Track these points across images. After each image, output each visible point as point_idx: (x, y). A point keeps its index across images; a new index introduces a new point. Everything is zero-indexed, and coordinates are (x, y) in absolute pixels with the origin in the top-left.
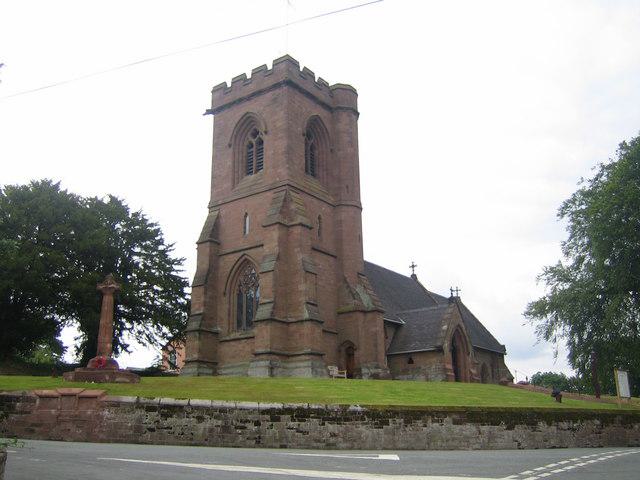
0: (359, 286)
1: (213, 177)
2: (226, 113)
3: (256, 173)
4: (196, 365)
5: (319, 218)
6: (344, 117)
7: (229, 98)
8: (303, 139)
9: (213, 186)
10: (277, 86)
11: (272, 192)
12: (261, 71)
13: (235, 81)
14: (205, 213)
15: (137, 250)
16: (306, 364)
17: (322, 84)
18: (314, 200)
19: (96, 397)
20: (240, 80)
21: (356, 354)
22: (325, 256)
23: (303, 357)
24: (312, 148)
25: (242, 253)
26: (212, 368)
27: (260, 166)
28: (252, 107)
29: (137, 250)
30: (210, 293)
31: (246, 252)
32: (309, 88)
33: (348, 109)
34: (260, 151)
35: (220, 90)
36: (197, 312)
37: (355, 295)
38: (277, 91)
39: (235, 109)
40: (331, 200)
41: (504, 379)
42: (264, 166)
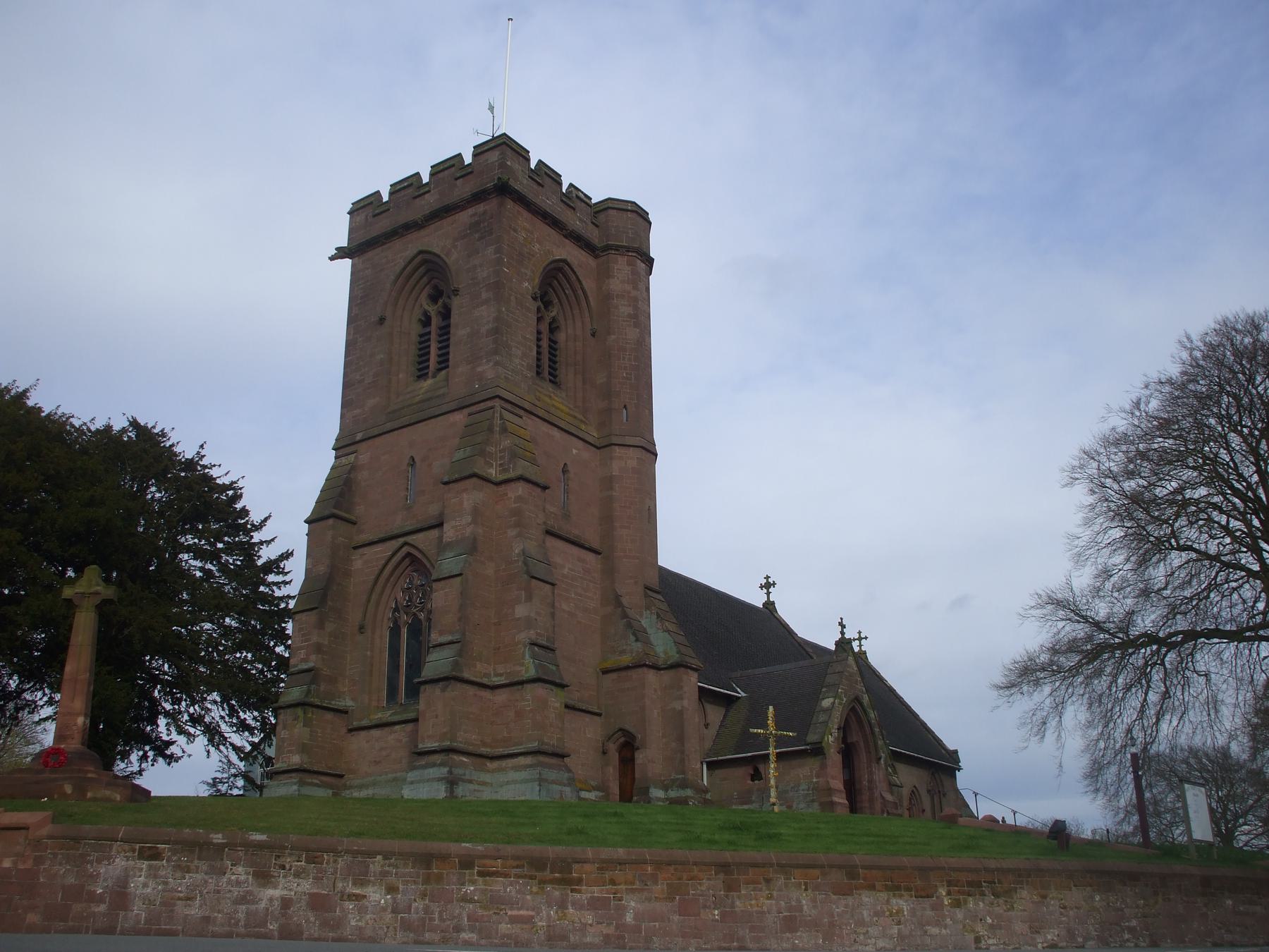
0: (646, 613)
1: (347, 385)
2: (375, 254)
3: (434, 376)
4: (295, 778)
5: (565, 471)
6: (621, 266)
7: (384, 224)
8: (533, 306)
9: (346, 404)
10: (478, 197)
11: (466, 411)
12: (448, 169)
13: (397, 189)
14: (327, 459)
15: (190, 540)
16: (523, 775)
17: (575, 197)
18: (556, 433)
19: (26, 828)
20: (408, 187)
21: (640, 757)
22: (575, 550)
23: (522, 760)
24: (553, 328)
25: (402, 540)
26: (330, 786)
27: (444, 362)
28: (436, 239)
29: (190, 540)
30: (330, 627)
31: (409, 539)
32: (549, 203)
33: (628, 249)
34: (445, 331)
35: (366, 209)
36: (304, 666)
37: (640, 634)
38: (481, 208)
39: (397, 244)
40: (593, 434)
41: (948, 810)
42: (451, 363)
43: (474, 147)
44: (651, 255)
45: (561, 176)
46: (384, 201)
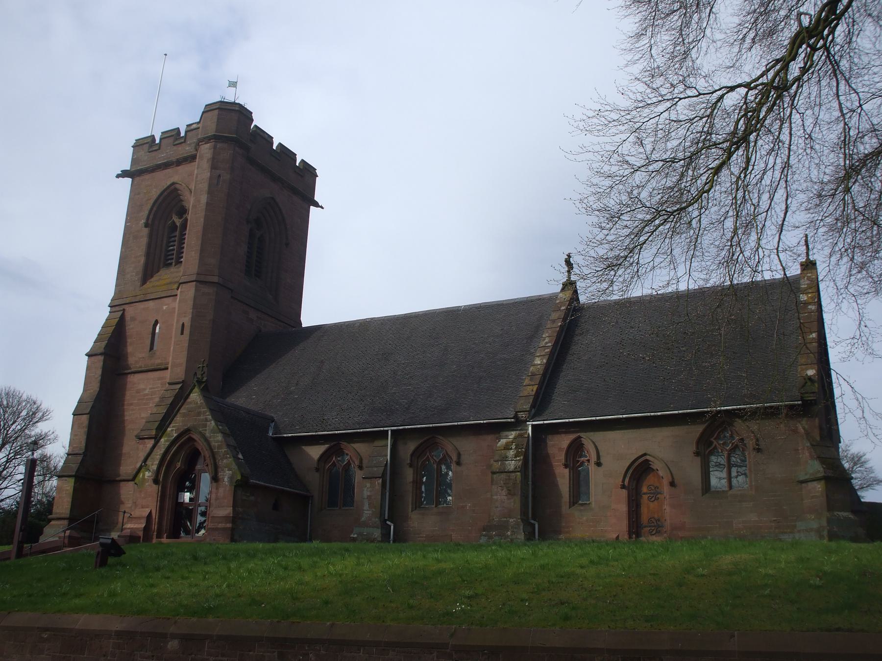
35: (144, 145)
39: (159, 175)
43: (162, 133)
44: (315, 199)
45: (273, 138)
46: (181, 136)
